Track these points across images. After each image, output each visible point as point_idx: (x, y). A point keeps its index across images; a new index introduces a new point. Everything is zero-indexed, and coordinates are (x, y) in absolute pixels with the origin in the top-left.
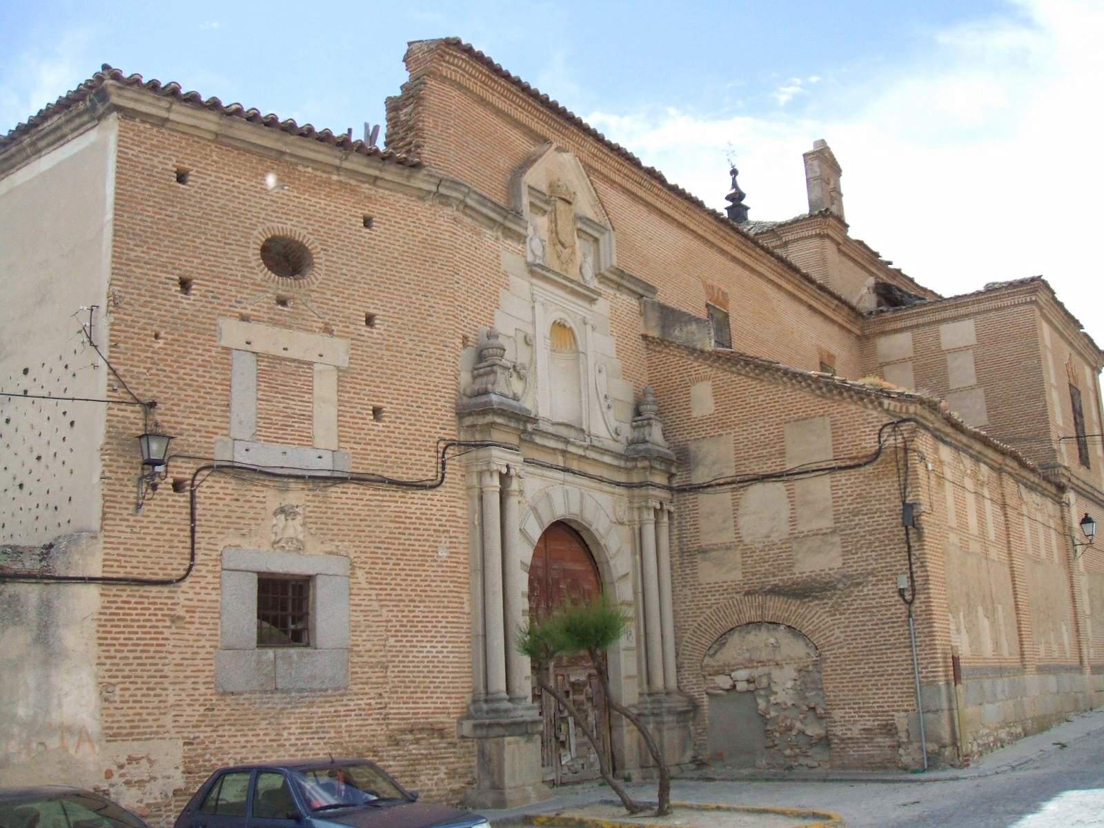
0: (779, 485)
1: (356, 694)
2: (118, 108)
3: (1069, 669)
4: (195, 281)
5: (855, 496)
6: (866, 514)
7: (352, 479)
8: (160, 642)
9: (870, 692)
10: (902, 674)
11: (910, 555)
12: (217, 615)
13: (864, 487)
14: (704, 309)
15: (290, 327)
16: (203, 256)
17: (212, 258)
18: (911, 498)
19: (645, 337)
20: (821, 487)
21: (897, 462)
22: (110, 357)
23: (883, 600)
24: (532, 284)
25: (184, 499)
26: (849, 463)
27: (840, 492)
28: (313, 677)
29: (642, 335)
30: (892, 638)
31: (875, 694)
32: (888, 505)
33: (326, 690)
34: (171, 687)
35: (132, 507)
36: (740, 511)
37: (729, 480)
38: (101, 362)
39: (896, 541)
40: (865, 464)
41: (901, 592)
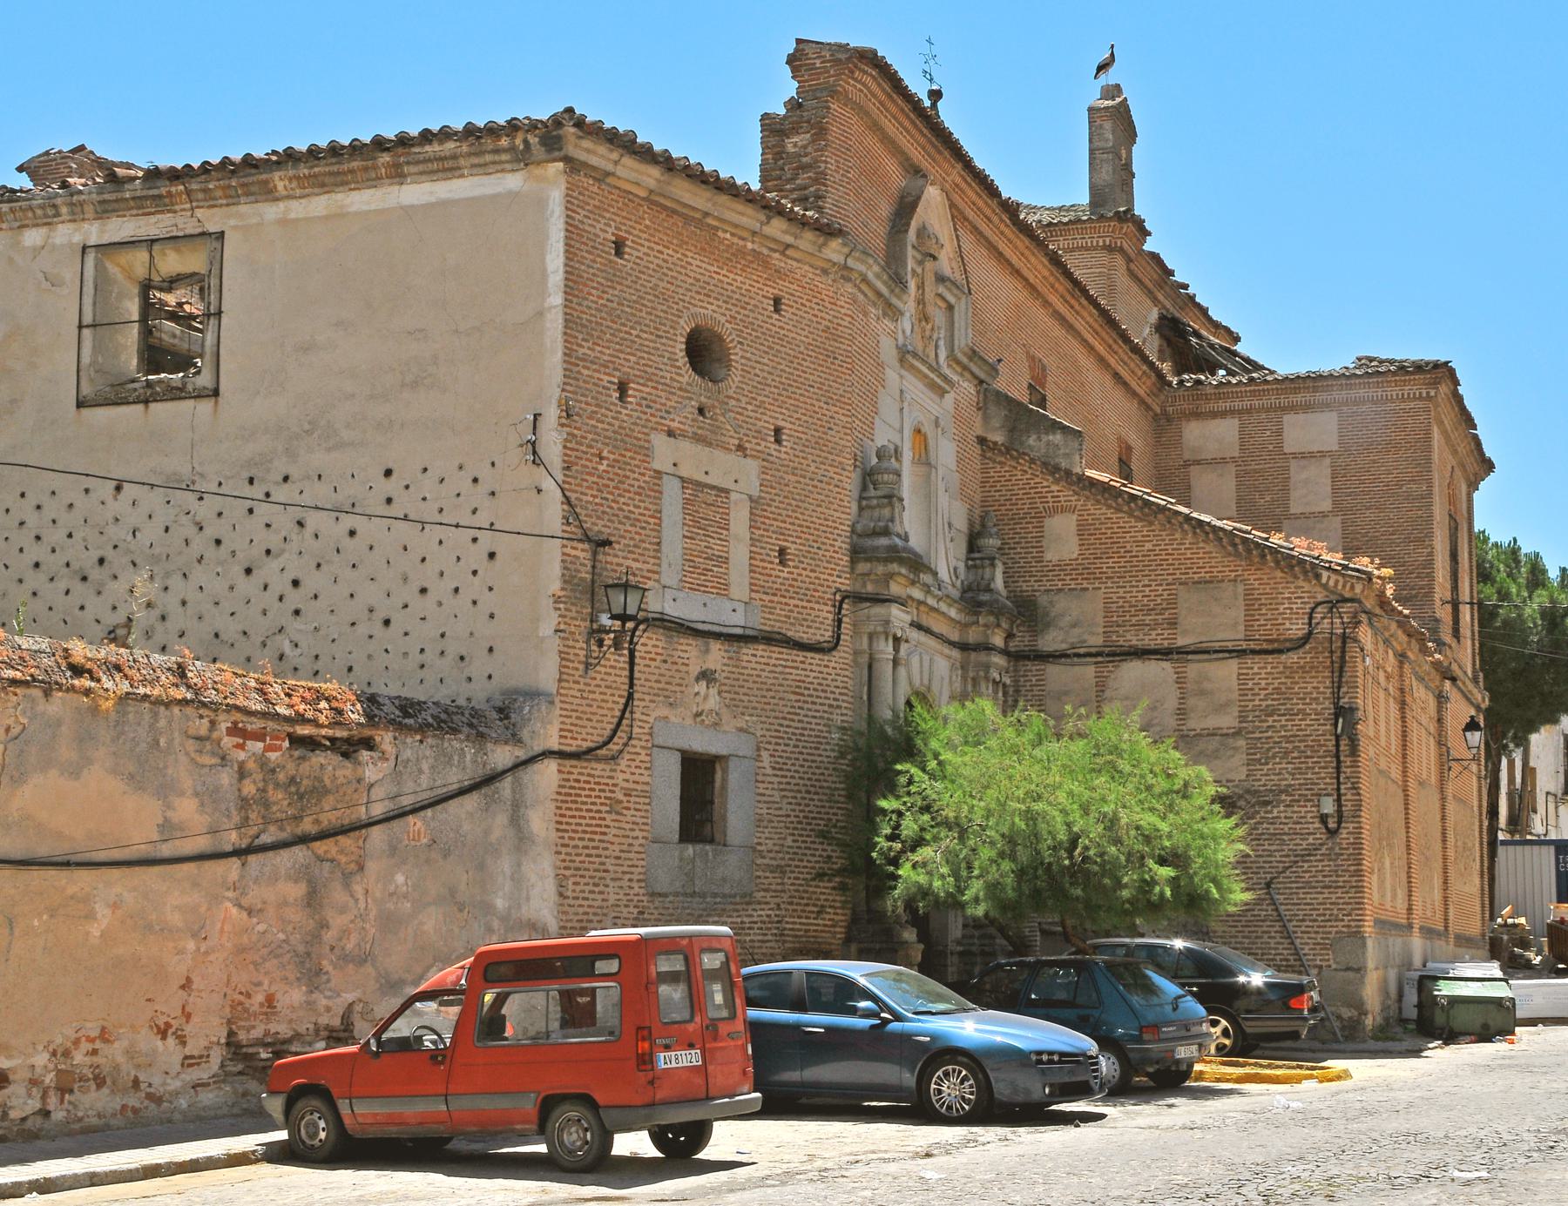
0: (1166, 665)
1: (759, 903)
2: (567, 159)
3: (1397, 926)
4: (632, 385)
5: (1270, 691)
6: (1284, 715)
7: (763, 638)
8: (603, 830)
9: (1272, 941)
10: (1315, 920)
11: (1338, 773)
12: (647, 801)
13: (1283, 680)
14: (1026, 392)
15: (710, 445)
16: (639, 354)
17: (646, 356)
18: (1346, 700)
19: (982, 441)
20: (1226, 673)
21: (1332, 652)
22: (564, 482)
23: (1298, 826)
24: (901, 377)
25: (622, 659)
26: (1265, 646)
27: (1250, 683)
28: (724, 880)
29: (978, 437)
30: (1307, 875)
31: (1278, 943)
32: (1314, 706)
33: (735, 896)
34: (612, 884)
35: (581, 667)
36: (1108, 694)
37: (1093, 650)
38: (549, 485)
39: (1321, 753)
40: (1289, 650)
41: (1323, 819)
